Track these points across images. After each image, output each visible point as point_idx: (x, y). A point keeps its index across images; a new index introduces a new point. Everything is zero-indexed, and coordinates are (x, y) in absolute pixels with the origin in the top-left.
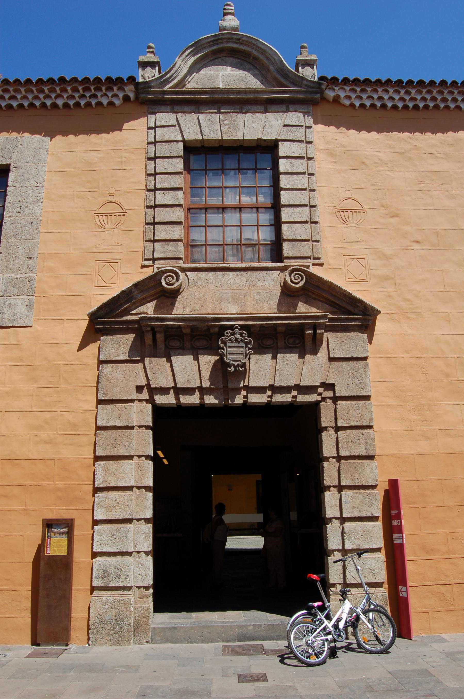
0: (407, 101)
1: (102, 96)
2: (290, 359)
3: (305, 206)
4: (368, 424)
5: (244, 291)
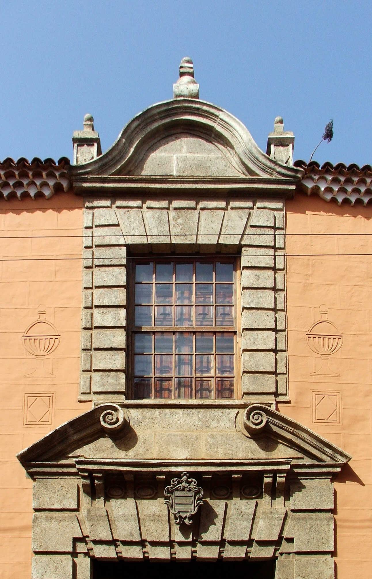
5: (195, 434)
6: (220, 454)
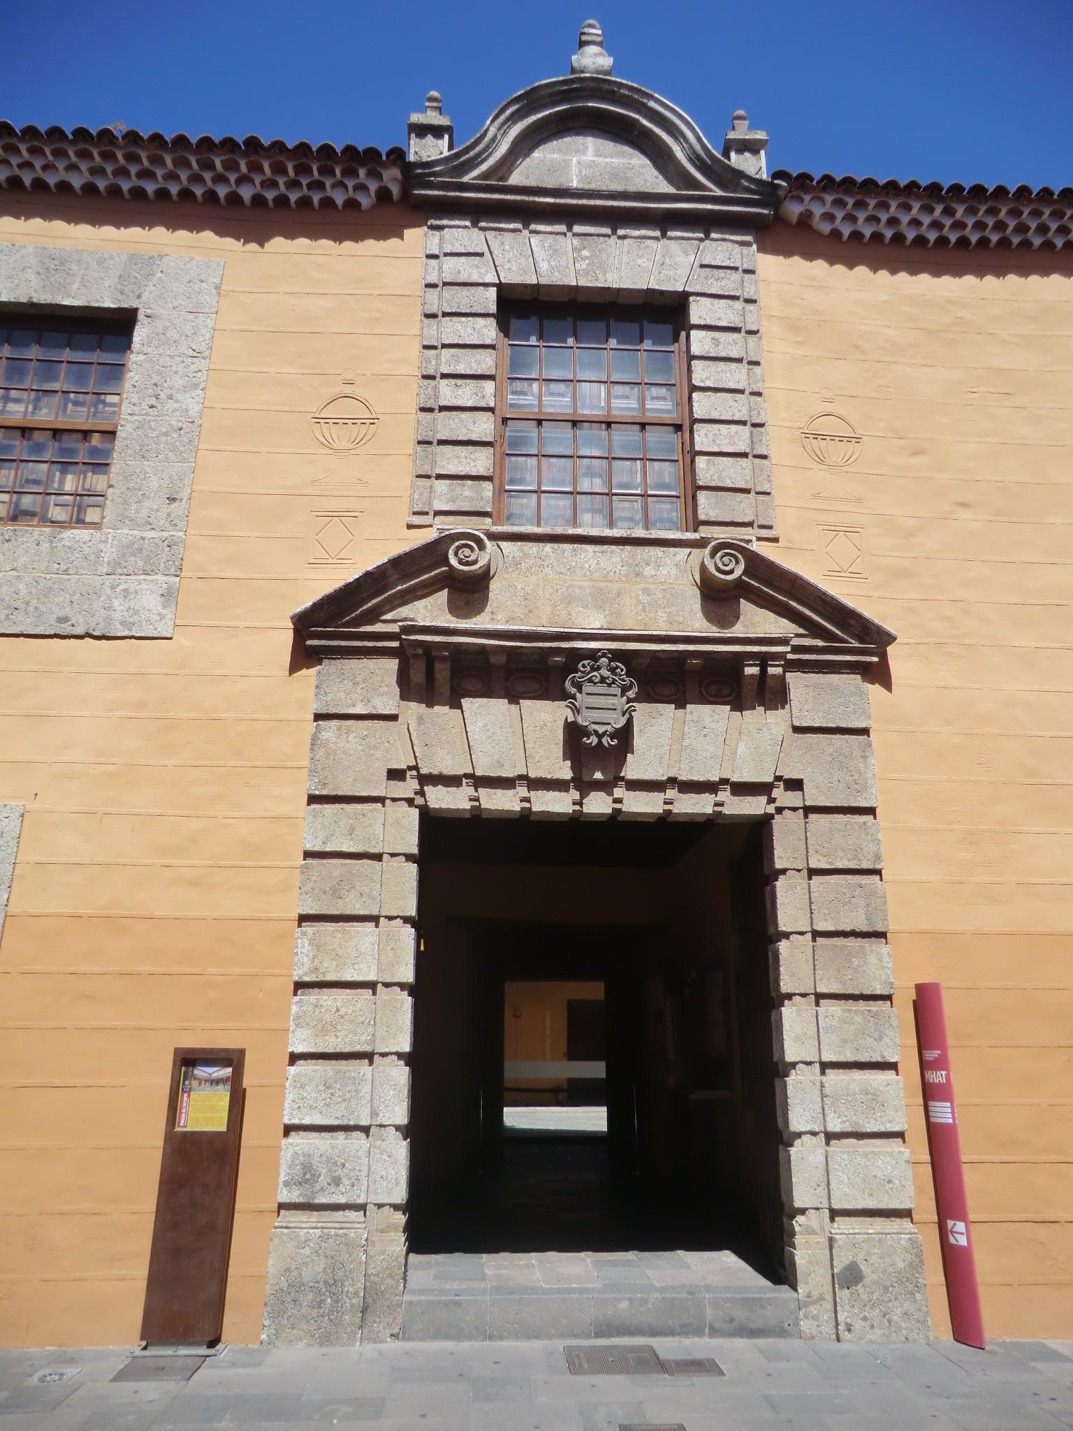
0: (946, 229)
1: (333, 186)
2: (713, 725)
4: (871, 867)
5: (617, 586)
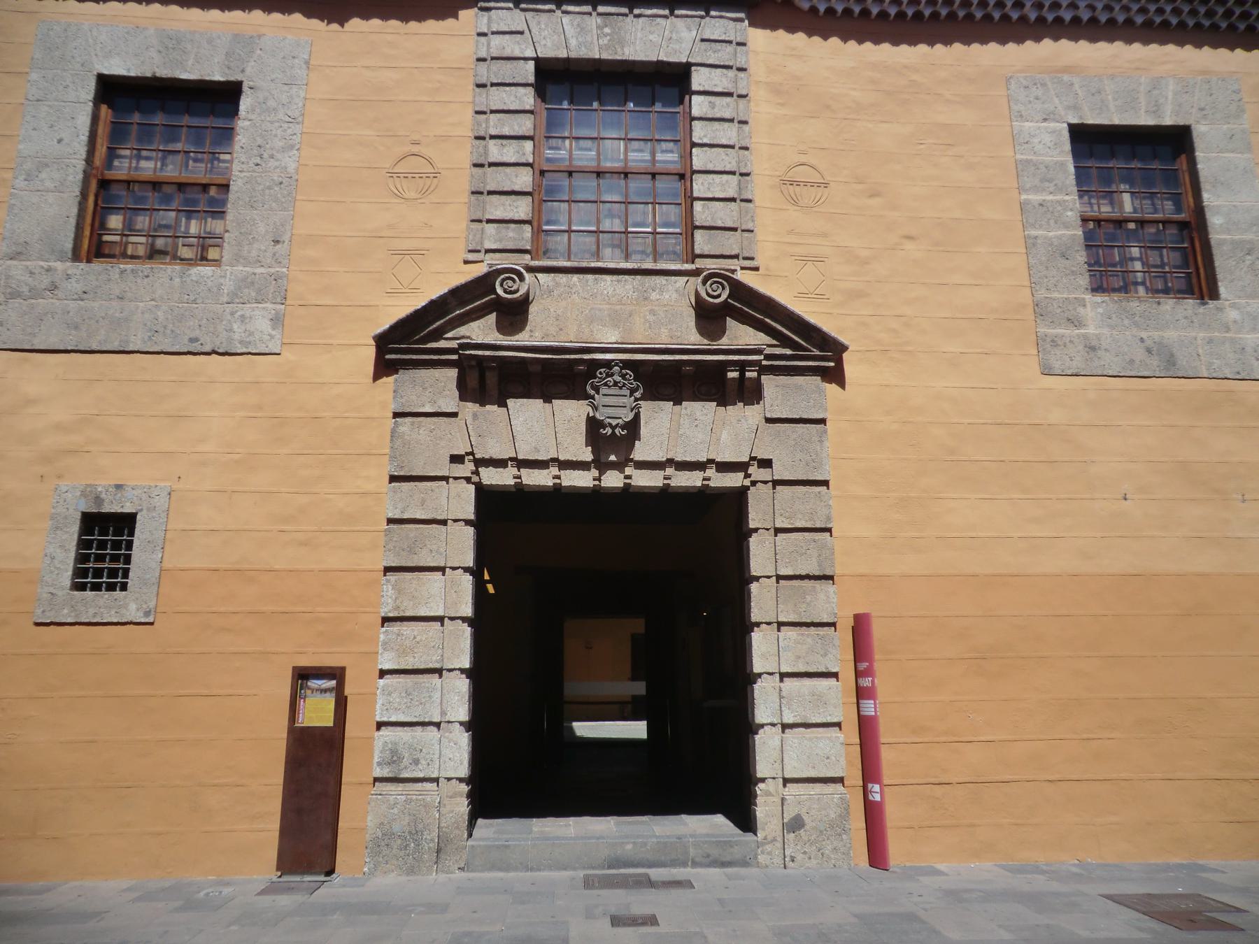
3: (733, 173)
6: (663, 338)
